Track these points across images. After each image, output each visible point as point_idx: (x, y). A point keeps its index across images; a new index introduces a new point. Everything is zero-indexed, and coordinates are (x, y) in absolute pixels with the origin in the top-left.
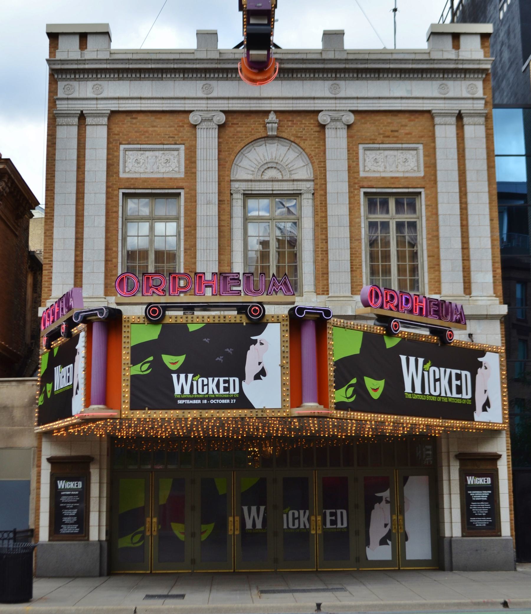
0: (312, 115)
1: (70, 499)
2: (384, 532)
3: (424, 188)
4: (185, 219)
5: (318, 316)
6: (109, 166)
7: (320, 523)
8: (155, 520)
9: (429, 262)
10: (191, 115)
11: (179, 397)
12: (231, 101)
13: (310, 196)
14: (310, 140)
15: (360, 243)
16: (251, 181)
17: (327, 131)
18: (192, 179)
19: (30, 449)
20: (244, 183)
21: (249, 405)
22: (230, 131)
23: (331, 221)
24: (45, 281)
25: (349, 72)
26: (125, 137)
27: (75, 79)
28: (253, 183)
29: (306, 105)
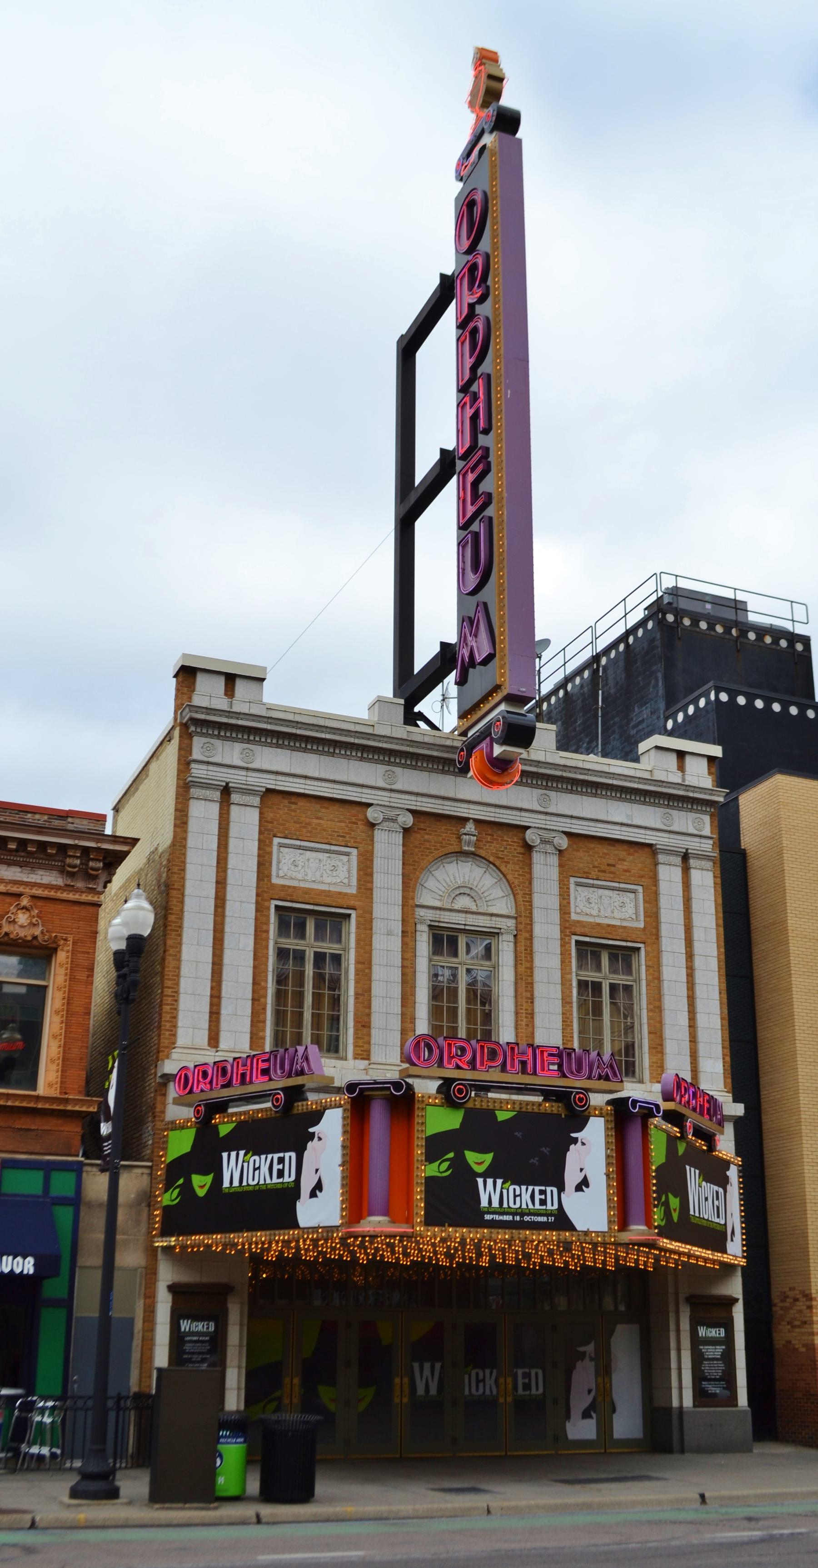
0: (358, 808)
1: (198, 1348)
2: (588, 1400)
3: (355, 909)
4: (356, 952)
5: (646, 1111)
6: (260, 865)
7: (510, 1387)
8: (296, 1381)
9: (650, 1040)
10: (370, 810)
11: (486, 1210)
12: (420, 799)
13: (512, 938)
14: (513, 863)
15: (572, 1007)
16: (440, 909)
17: (376, 832)
18: (367, 898)
19: (136, 1270)
20: (431, 911)
21: (570, 1227)
22: (416, 837)
23: (538, 976)
24: (166, 1021)
25: (562, 782)
26: (281, 827)
27: (218, 737)
28: (442, 913)
29: (510, 817)
